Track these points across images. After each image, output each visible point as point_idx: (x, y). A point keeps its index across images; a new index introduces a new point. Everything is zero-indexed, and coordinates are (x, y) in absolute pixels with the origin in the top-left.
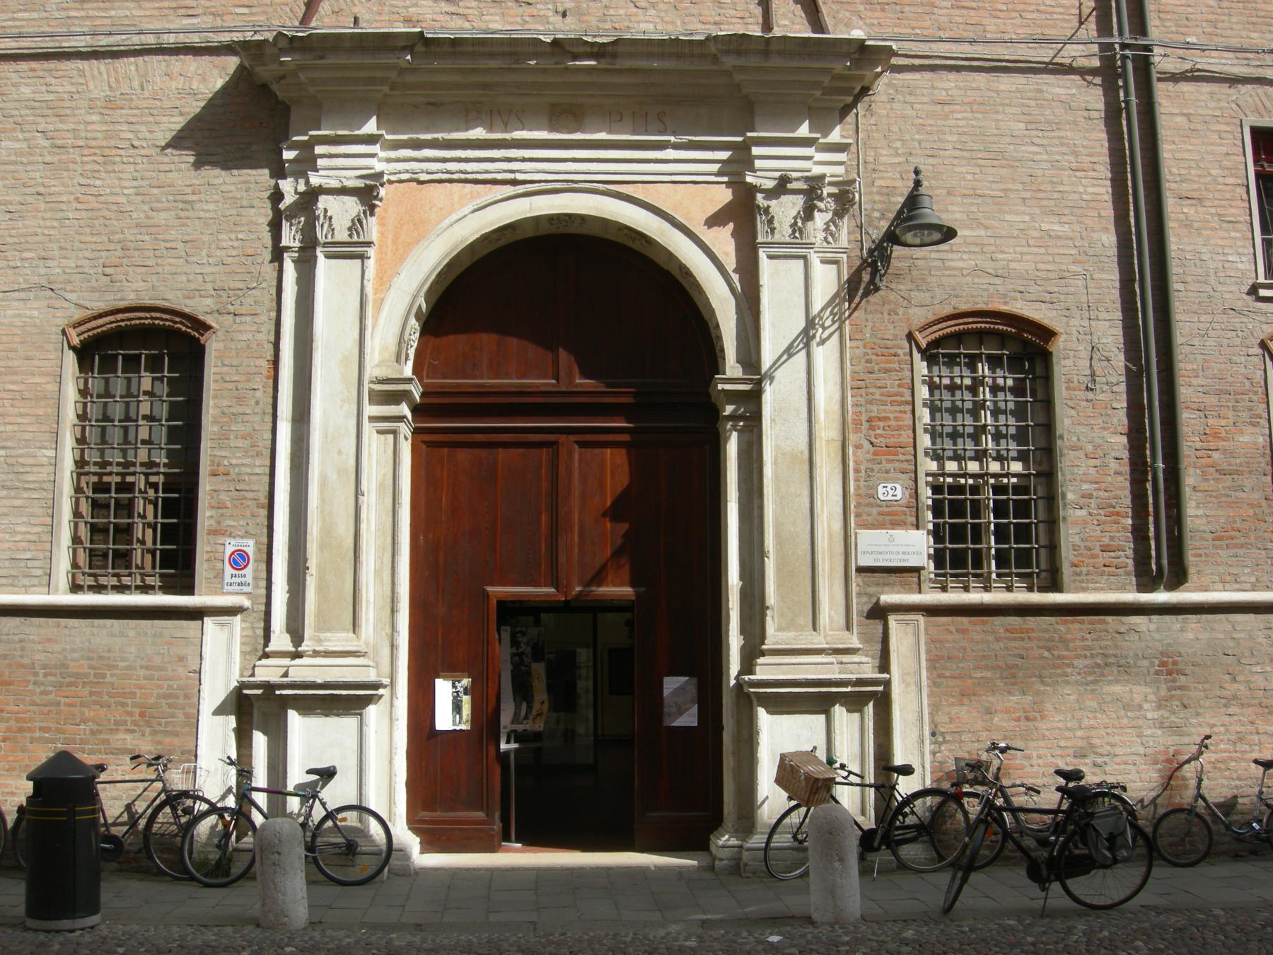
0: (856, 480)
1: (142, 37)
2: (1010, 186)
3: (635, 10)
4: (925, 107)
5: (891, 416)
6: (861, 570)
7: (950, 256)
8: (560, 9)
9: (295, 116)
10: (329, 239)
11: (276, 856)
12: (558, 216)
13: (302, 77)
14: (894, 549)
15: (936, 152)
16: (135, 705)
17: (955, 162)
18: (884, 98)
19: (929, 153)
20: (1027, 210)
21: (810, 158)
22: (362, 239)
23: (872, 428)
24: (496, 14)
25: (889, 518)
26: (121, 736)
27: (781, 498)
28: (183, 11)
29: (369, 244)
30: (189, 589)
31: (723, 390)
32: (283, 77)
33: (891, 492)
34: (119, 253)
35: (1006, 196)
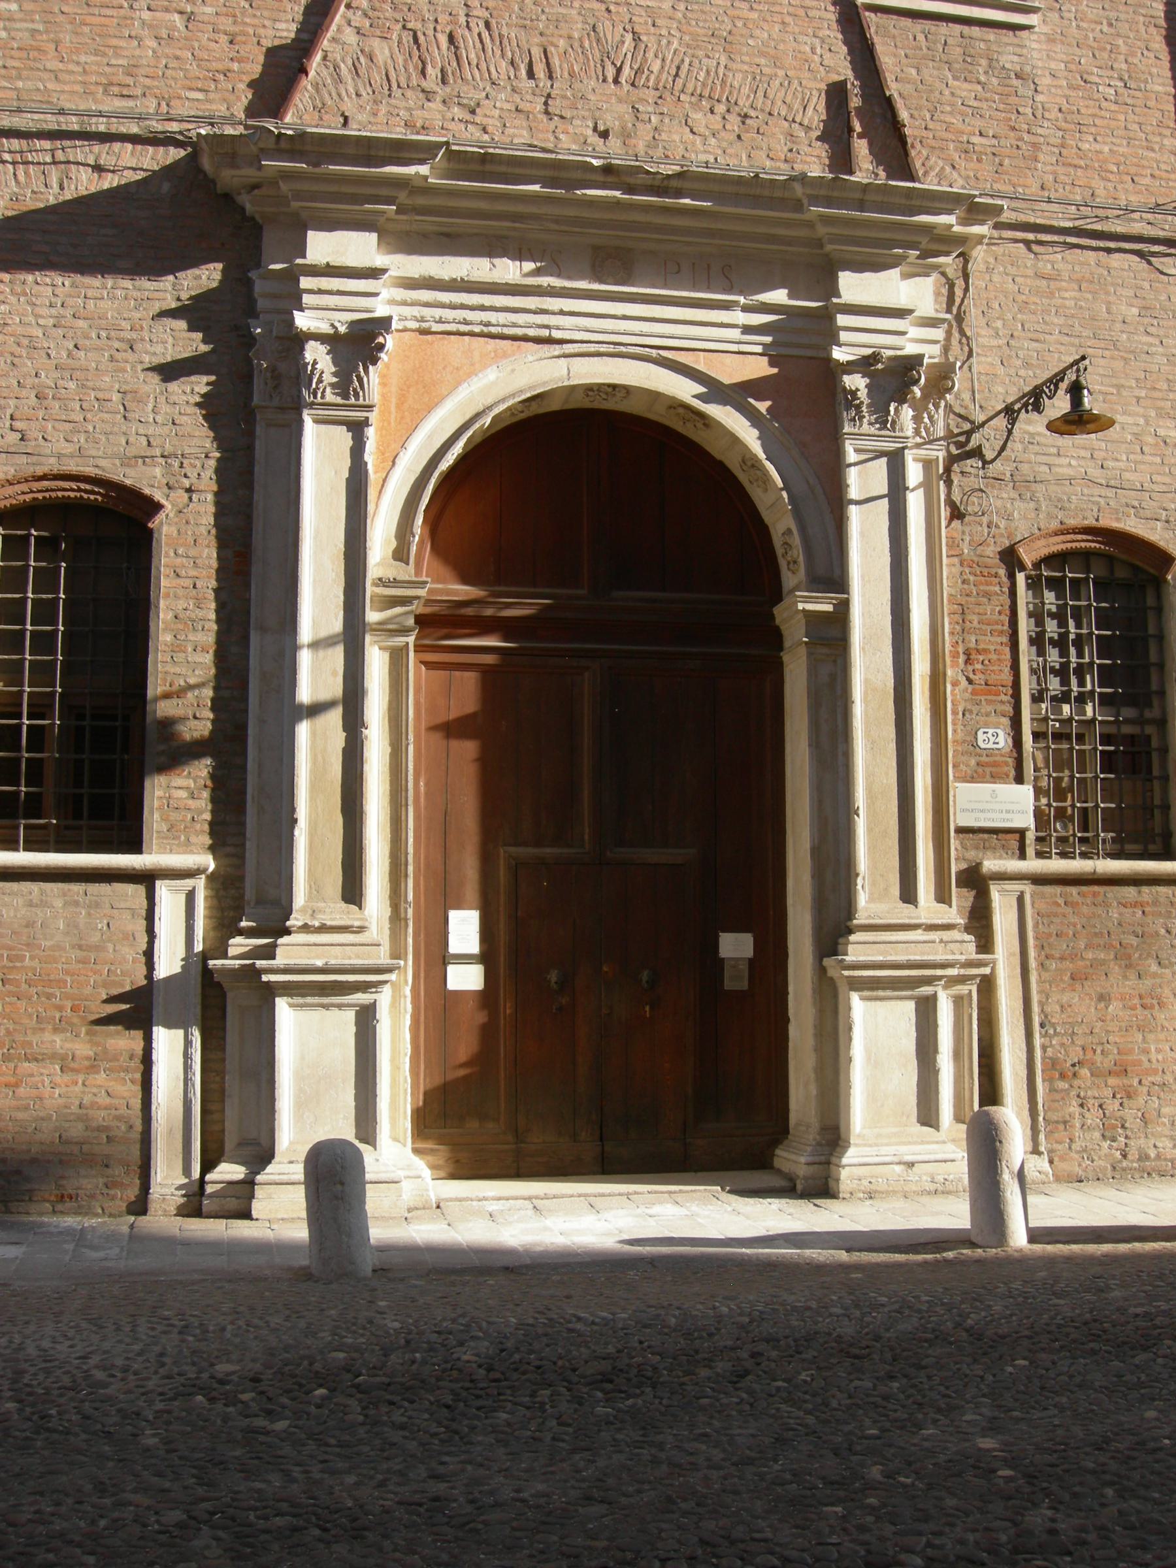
0: (954, 724)
1: (62, 119)
2: (1123, 381)
3: (691, 136)
4: (1029, 281)
5: (992, 648)
6: (961, 830)
7: (1057, 461)
8: (601, 128)
9: (269, 238)
10: (319, 400)
11: (339, 1187)
12: (600, 386)
13: (284, 187)
14: (997, 807)
15: (1041, 337)
16: (67, 996)
17: (1062, 348)
18: (982, 267)
19: (1034, 336)
20: (1141, 411)
21: (903, 333)
22: (361, 401)
23: (968, 661)
24: (522, 128)
25: (986, 770)
26: (47, 1036)
27: (873, 742)
28: (116, 90)
29: (369, 407)
30: (135, 846)
31: (804, 610)
32: (255, 187)
33: (989, 735)
34: (33, 401)
35: (1119, 393)
